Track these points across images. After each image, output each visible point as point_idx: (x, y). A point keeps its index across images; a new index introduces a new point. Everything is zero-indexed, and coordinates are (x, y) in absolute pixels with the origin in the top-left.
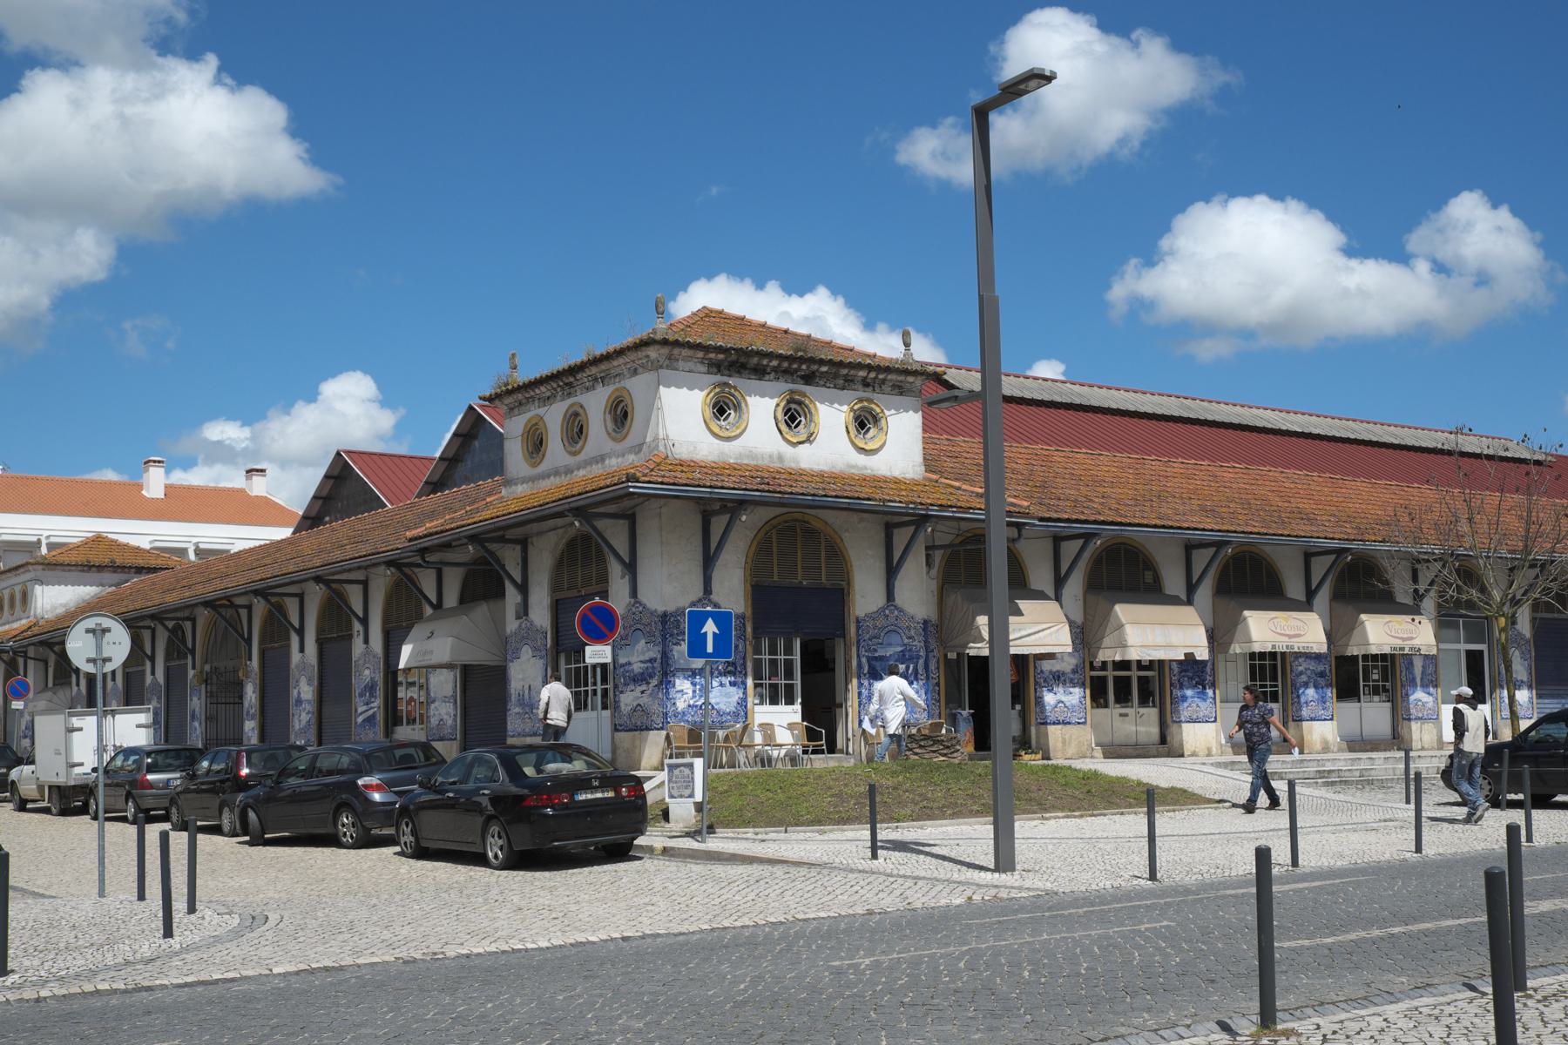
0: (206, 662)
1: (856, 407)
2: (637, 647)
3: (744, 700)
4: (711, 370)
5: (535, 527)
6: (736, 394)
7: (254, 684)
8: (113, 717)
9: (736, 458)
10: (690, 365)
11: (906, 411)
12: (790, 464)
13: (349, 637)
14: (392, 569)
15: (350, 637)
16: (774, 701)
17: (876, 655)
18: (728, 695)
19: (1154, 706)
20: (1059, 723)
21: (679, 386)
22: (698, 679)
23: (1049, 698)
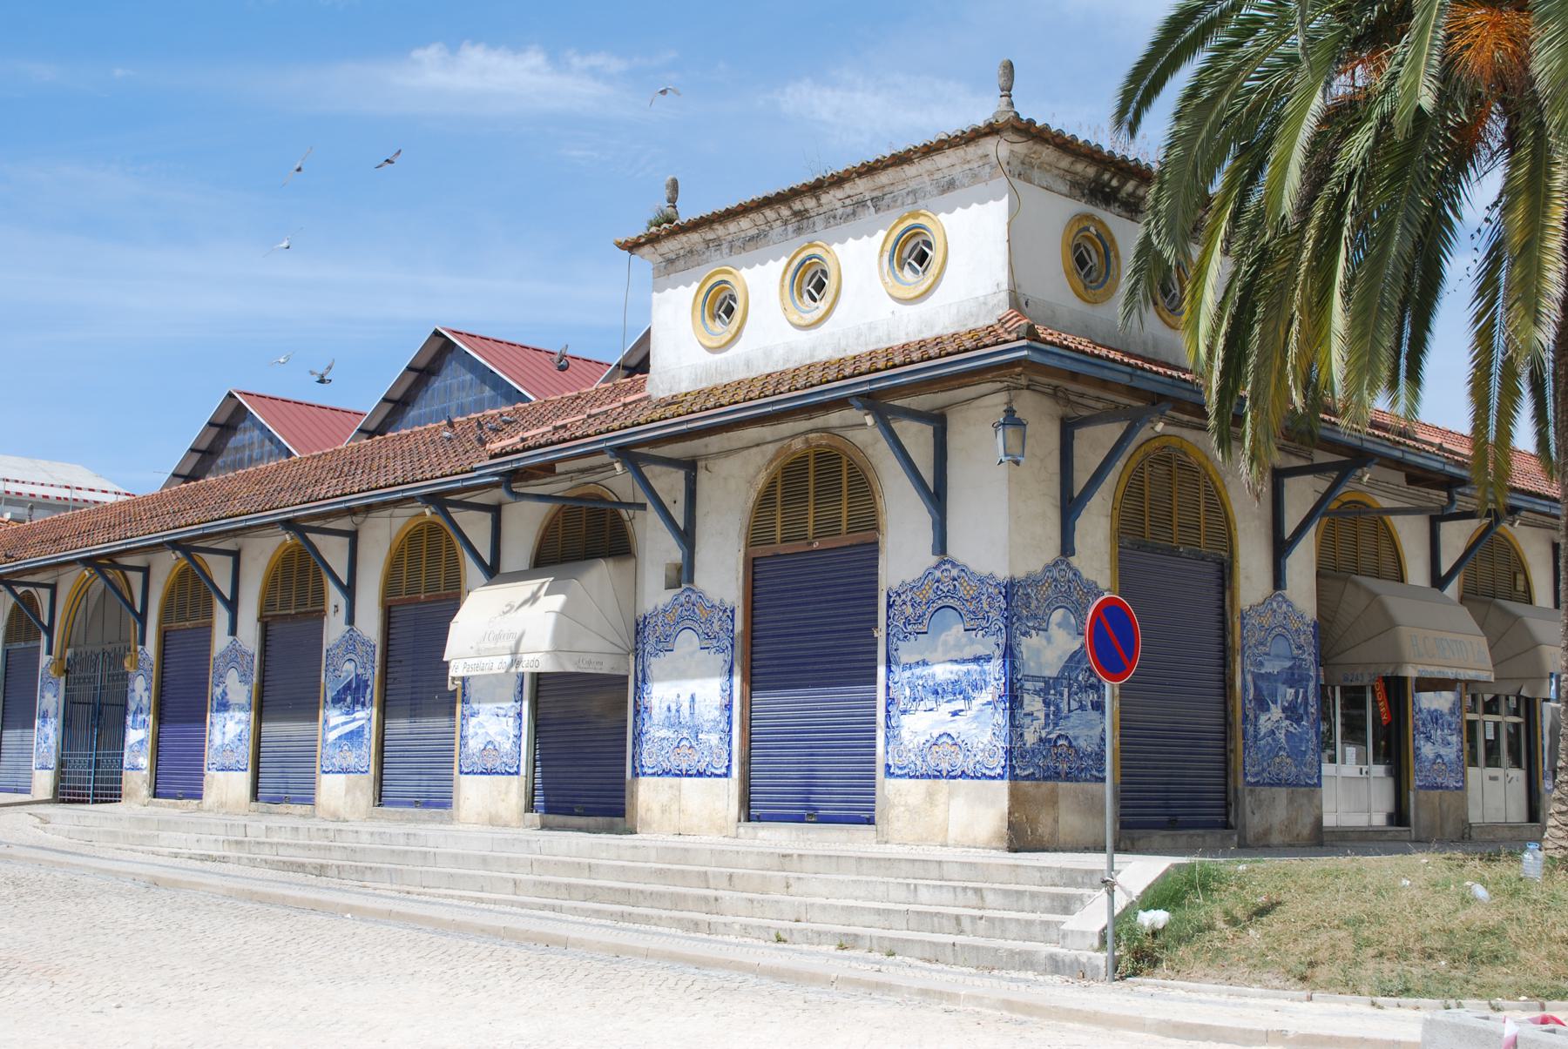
0: (68, 646)
2: (943, 637)
5: (715, 442)
7: (148, 679)
14: (178, 552)
15: (320, 615)
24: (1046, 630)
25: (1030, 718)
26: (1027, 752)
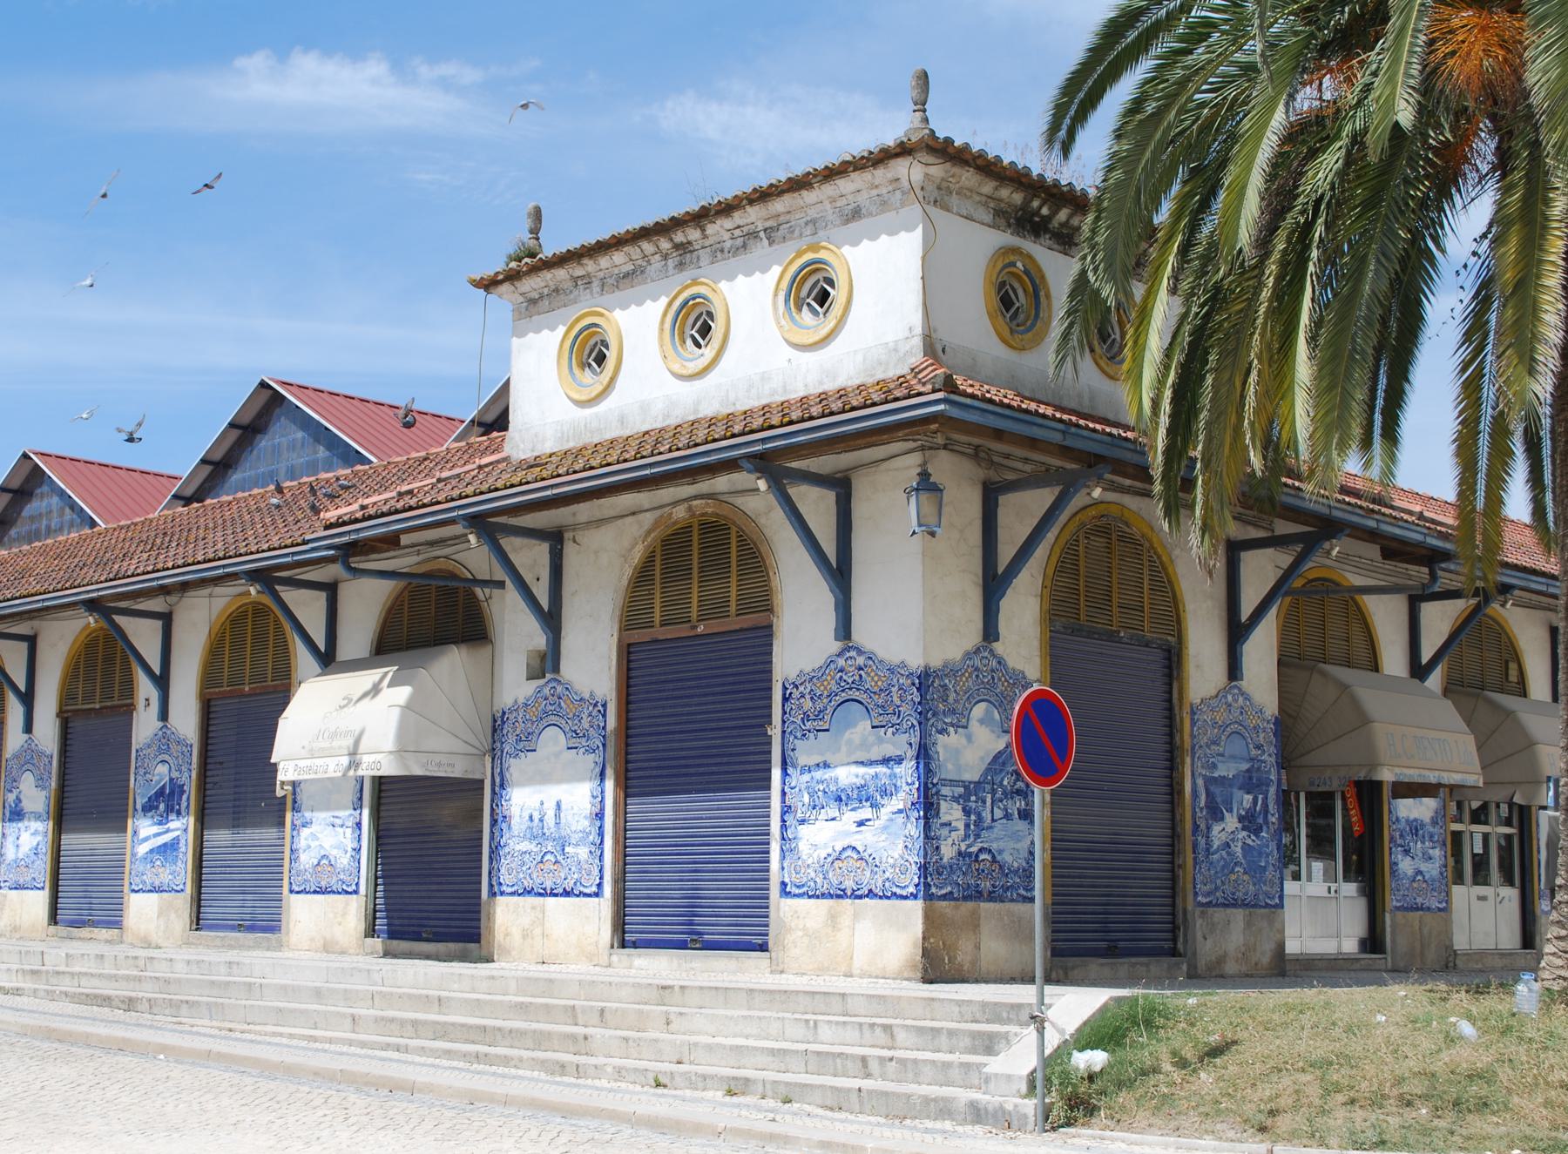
2: (847, 735)
5: (584, 511)
13: (126, 710)
15: (129, 709)
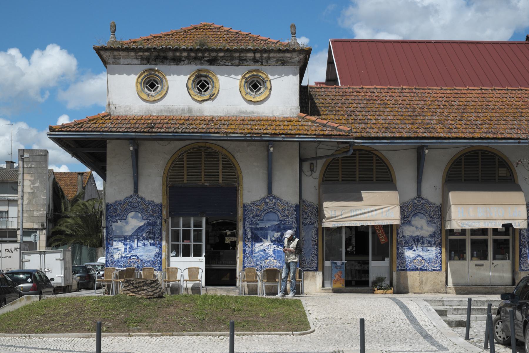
1: (247, 76)
3: (160, 254)
4: (143, 62)
6: (159, 75)
8: (45, 255)
9: (158, 113)
10: (129, 60)
11: (287, 75)
12: (196, 114)
16: (186, 254)
17: (258, 227)
18: (149, 251)
19: (509, 259)
20: (417, 270)
21: (120, 73)
22: (128, 242)
23: (409, 254)
24: (126, 220)
25: (117, 250)
26: (115, 261)
